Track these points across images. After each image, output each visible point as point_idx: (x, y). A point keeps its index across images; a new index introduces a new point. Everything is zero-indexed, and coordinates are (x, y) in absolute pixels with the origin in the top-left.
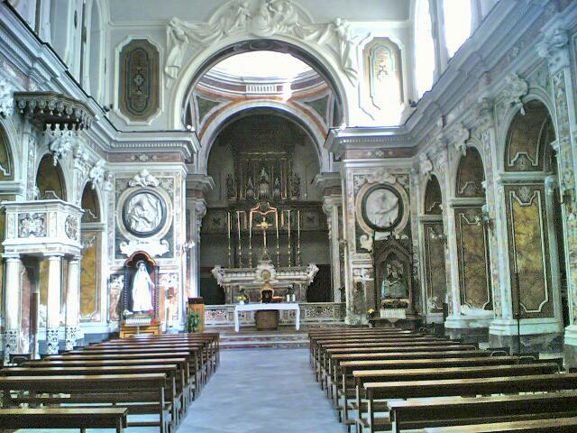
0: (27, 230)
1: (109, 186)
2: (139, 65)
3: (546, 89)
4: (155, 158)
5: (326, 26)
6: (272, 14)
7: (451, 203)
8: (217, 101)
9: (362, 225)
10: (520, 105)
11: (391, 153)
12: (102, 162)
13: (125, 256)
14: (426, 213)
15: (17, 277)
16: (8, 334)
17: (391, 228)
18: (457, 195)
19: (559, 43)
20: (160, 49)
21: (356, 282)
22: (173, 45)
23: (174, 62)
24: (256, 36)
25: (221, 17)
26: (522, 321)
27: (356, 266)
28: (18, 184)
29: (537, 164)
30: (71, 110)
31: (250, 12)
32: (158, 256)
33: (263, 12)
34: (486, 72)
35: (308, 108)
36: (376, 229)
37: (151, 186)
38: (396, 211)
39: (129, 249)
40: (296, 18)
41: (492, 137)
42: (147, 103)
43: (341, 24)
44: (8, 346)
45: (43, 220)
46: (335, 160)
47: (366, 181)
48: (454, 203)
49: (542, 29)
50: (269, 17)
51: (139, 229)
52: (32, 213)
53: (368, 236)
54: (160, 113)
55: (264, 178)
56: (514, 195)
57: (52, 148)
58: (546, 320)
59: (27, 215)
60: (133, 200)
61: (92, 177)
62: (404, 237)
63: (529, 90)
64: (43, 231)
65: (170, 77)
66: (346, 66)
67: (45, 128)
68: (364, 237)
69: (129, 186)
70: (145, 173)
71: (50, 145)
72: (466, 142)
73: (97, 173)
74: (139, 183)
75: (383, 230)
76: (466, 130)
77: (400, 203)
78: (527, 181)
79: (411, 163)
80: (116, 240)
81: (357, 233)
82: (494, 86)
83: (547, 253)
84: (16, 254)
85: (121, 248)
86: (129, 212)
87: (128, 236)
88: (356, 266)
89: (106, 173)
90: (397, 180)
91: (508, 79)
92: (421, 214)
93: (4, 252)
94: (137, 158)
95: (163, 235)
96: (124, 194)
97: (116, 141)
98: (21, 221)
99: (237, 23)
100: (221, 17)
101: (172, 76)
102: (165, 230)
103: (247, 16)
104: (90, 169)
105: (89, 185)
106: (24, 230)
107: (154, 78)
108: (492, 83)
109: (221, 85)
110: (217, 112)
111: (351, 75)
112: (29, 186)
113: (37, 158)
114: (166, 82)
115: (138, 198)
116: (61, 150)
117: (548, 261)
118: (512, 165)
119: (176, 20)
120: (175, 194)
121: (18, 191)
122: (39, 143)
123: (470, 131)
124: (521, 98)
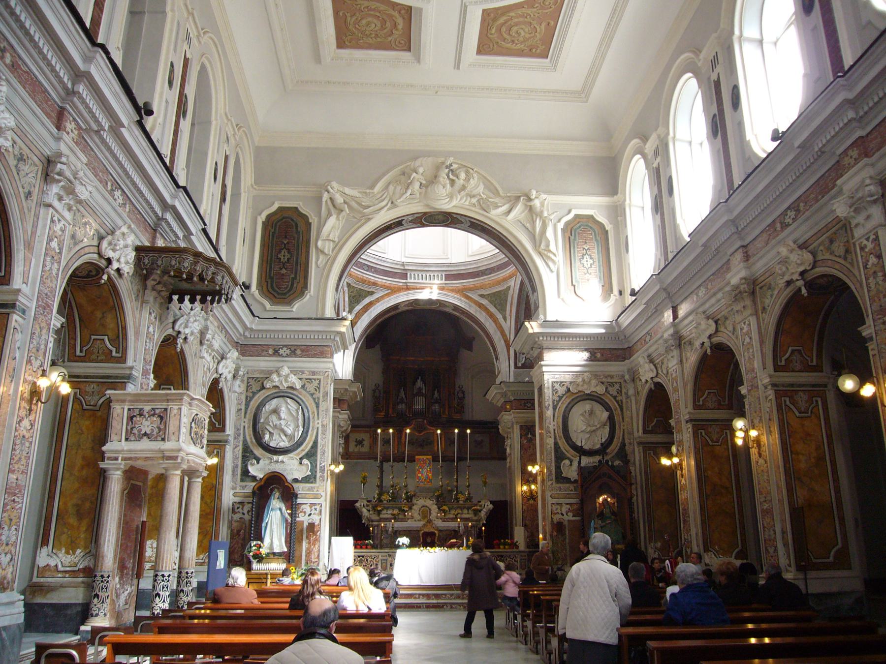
0: (140, 431)
1: (238, 387)
2: (286, 237)
3: (845, 259)
4: (298, 352)
5: (518, 198)
6: (452, 182)
7: (687, 417)
8: (372, 289)
9: (564, 446)
10: (800, 283)
11: (599, 355)
12: (234, 354)
13: (254, 478)
14: (645, 432)
15: (119, 496)
16: (99, 578)
17: (606, 446)
18: (696, 406)
19: (872, 196)
20: (313, 220)
21: (555, 521)
22: (329, 215)
23: (329, 235)
24: (435, 208)
25: (389, 184)
26: (812, 574)
27: (554, 501)
28: (131, 368)
29: (814, 363)
30: (210, 273)
31: (425, 180)
32: (296, 480)
33: (441, 179)
34: (743, 246)
35: (484, 302)
36: (581, 451)
37: (292, 388)
38: (607, 429)
39: (257, 470)
40: (481, 189)
41: (754, 327)
42: (292, 284)
43: (536, 197)
44: (97, 596)
45: (161, 418)
46: (516, 367)
47: (568, 390)
48: (693, 417)
49: (839, 182)
50: (448, 186)
51: (273, 444)
52: (147, 408)
53: (571, 461)
54: (308, 297)
55: (420, 389)
56: (788, 403)
57: (177, 328)
58: (839, 573)
59: (141, 410)
60: (267, 406)
61: (220, 372)
62: (617, 463)
63: (815, 262)
64: (162, 434)
65: (323, 252)
66: (543, 246)
67: (170, 300)
68: (567, 462)
69: (263, 388)
70: (285, 371)
71: (174, 323)
72: (710, 337)
73: (226, 369)
74: (277, 384)
75: (590, 453)
76: (711, 322)
77: (611, 418)
78: (804, 385)
79: (625, 368)
80: (244, 457)
81: (556, 457)
82: (754, 264)
83: (836, 480)
84: (122, 464)
85: (250, 468)
86: (262, 421)
87: (258, 452)
88: (554, 501)
89: (237, 370)
90: (607, 388)
91: (784, 251)
92: (639, 433)
93: (103, 460)
94: (276, 353)
95: (304, 453)
96: (257, 396)
97: (251, 330)
98: (131, 418)
99: (409, 192)
100: (389, 184)
101: (326, 252)
102: (306, 447)
103: (421, 183)
104: (218, 363)
105: (216, 382)
106: (135, 431)
107: (304, 250)
108: (751, 260)
109: (377, 271)
110: (371, 304)
111: (549, 258)
112: (145, 373)
113: (158, 338)
114: (317, 260)
115: (274, 402)
116: (187, 331)
117: (838, 492)
118: (783, 363)
119: (334, 184)
120: (321, 398)
121: (129, 377)
122: (161, 319)
123: (716, 322)
124: (802, 274)
